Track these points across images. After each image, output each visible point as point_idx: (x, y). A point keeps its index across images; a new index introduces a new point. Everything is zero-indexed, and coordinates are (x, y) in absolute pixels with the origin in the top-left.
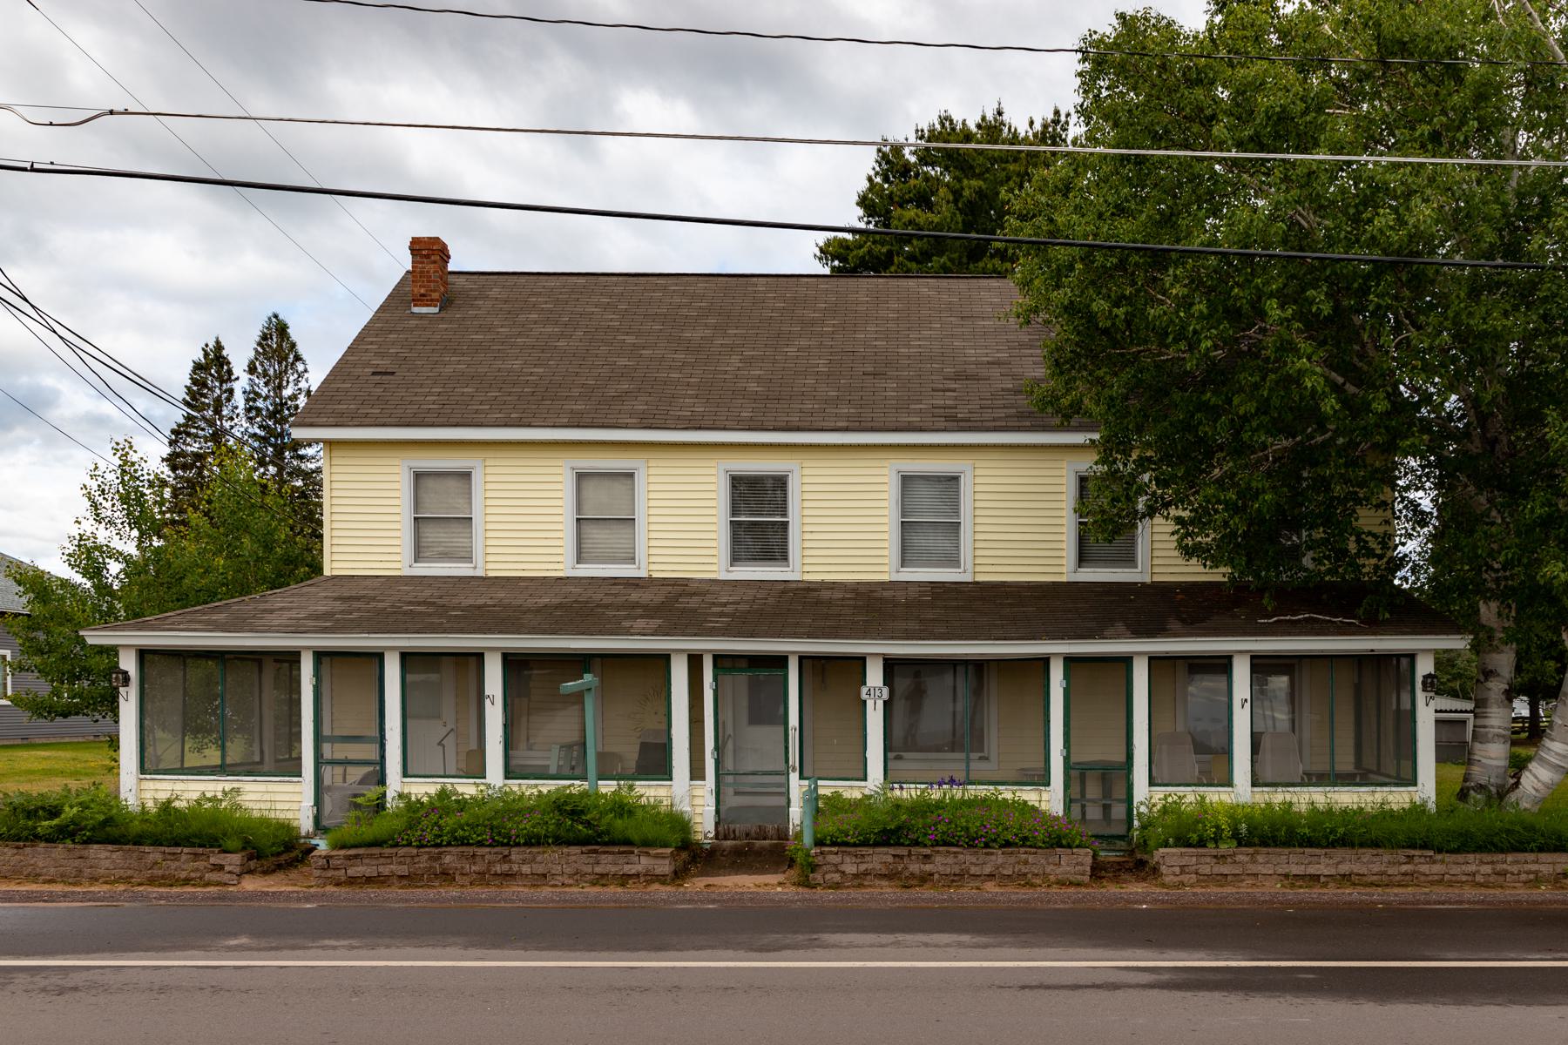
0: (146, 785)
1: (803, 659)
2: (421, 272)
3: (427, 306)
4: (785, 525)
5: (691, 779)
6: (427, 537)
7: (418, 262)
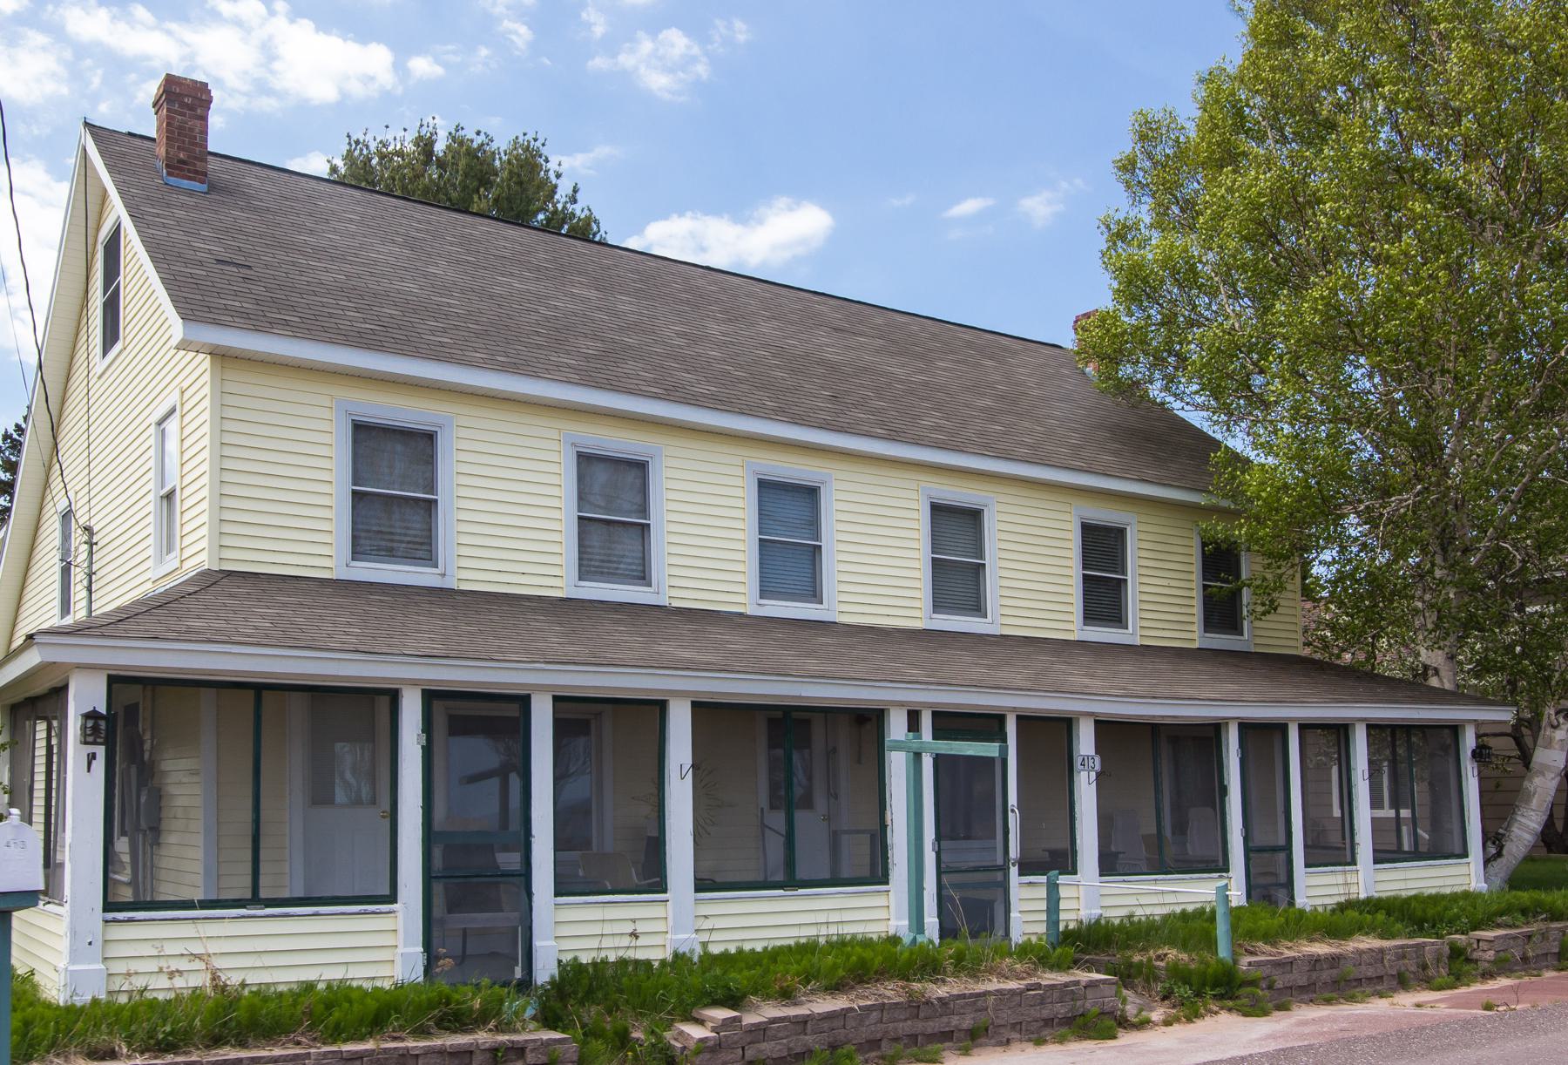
0: (118, 932)
1: (1373, 728)
2: (180, 128)
3: (190, 179)
4: (431, 505)
5: (557, 895)
6: (590, 547)
7: (176, 112)
